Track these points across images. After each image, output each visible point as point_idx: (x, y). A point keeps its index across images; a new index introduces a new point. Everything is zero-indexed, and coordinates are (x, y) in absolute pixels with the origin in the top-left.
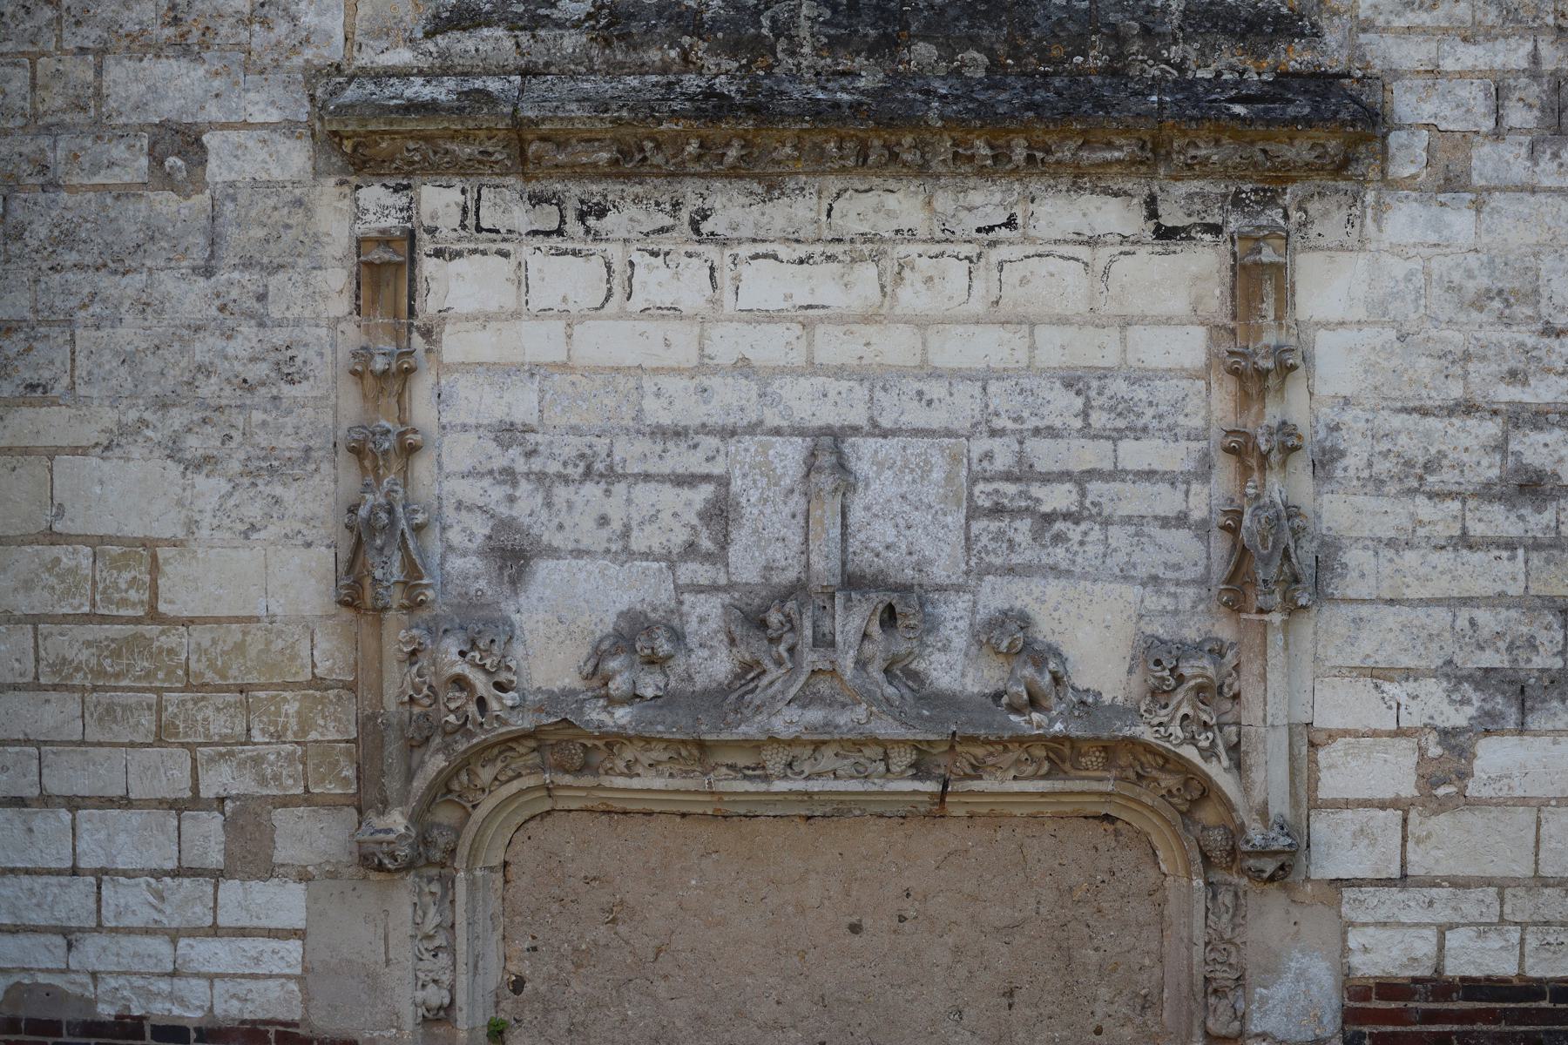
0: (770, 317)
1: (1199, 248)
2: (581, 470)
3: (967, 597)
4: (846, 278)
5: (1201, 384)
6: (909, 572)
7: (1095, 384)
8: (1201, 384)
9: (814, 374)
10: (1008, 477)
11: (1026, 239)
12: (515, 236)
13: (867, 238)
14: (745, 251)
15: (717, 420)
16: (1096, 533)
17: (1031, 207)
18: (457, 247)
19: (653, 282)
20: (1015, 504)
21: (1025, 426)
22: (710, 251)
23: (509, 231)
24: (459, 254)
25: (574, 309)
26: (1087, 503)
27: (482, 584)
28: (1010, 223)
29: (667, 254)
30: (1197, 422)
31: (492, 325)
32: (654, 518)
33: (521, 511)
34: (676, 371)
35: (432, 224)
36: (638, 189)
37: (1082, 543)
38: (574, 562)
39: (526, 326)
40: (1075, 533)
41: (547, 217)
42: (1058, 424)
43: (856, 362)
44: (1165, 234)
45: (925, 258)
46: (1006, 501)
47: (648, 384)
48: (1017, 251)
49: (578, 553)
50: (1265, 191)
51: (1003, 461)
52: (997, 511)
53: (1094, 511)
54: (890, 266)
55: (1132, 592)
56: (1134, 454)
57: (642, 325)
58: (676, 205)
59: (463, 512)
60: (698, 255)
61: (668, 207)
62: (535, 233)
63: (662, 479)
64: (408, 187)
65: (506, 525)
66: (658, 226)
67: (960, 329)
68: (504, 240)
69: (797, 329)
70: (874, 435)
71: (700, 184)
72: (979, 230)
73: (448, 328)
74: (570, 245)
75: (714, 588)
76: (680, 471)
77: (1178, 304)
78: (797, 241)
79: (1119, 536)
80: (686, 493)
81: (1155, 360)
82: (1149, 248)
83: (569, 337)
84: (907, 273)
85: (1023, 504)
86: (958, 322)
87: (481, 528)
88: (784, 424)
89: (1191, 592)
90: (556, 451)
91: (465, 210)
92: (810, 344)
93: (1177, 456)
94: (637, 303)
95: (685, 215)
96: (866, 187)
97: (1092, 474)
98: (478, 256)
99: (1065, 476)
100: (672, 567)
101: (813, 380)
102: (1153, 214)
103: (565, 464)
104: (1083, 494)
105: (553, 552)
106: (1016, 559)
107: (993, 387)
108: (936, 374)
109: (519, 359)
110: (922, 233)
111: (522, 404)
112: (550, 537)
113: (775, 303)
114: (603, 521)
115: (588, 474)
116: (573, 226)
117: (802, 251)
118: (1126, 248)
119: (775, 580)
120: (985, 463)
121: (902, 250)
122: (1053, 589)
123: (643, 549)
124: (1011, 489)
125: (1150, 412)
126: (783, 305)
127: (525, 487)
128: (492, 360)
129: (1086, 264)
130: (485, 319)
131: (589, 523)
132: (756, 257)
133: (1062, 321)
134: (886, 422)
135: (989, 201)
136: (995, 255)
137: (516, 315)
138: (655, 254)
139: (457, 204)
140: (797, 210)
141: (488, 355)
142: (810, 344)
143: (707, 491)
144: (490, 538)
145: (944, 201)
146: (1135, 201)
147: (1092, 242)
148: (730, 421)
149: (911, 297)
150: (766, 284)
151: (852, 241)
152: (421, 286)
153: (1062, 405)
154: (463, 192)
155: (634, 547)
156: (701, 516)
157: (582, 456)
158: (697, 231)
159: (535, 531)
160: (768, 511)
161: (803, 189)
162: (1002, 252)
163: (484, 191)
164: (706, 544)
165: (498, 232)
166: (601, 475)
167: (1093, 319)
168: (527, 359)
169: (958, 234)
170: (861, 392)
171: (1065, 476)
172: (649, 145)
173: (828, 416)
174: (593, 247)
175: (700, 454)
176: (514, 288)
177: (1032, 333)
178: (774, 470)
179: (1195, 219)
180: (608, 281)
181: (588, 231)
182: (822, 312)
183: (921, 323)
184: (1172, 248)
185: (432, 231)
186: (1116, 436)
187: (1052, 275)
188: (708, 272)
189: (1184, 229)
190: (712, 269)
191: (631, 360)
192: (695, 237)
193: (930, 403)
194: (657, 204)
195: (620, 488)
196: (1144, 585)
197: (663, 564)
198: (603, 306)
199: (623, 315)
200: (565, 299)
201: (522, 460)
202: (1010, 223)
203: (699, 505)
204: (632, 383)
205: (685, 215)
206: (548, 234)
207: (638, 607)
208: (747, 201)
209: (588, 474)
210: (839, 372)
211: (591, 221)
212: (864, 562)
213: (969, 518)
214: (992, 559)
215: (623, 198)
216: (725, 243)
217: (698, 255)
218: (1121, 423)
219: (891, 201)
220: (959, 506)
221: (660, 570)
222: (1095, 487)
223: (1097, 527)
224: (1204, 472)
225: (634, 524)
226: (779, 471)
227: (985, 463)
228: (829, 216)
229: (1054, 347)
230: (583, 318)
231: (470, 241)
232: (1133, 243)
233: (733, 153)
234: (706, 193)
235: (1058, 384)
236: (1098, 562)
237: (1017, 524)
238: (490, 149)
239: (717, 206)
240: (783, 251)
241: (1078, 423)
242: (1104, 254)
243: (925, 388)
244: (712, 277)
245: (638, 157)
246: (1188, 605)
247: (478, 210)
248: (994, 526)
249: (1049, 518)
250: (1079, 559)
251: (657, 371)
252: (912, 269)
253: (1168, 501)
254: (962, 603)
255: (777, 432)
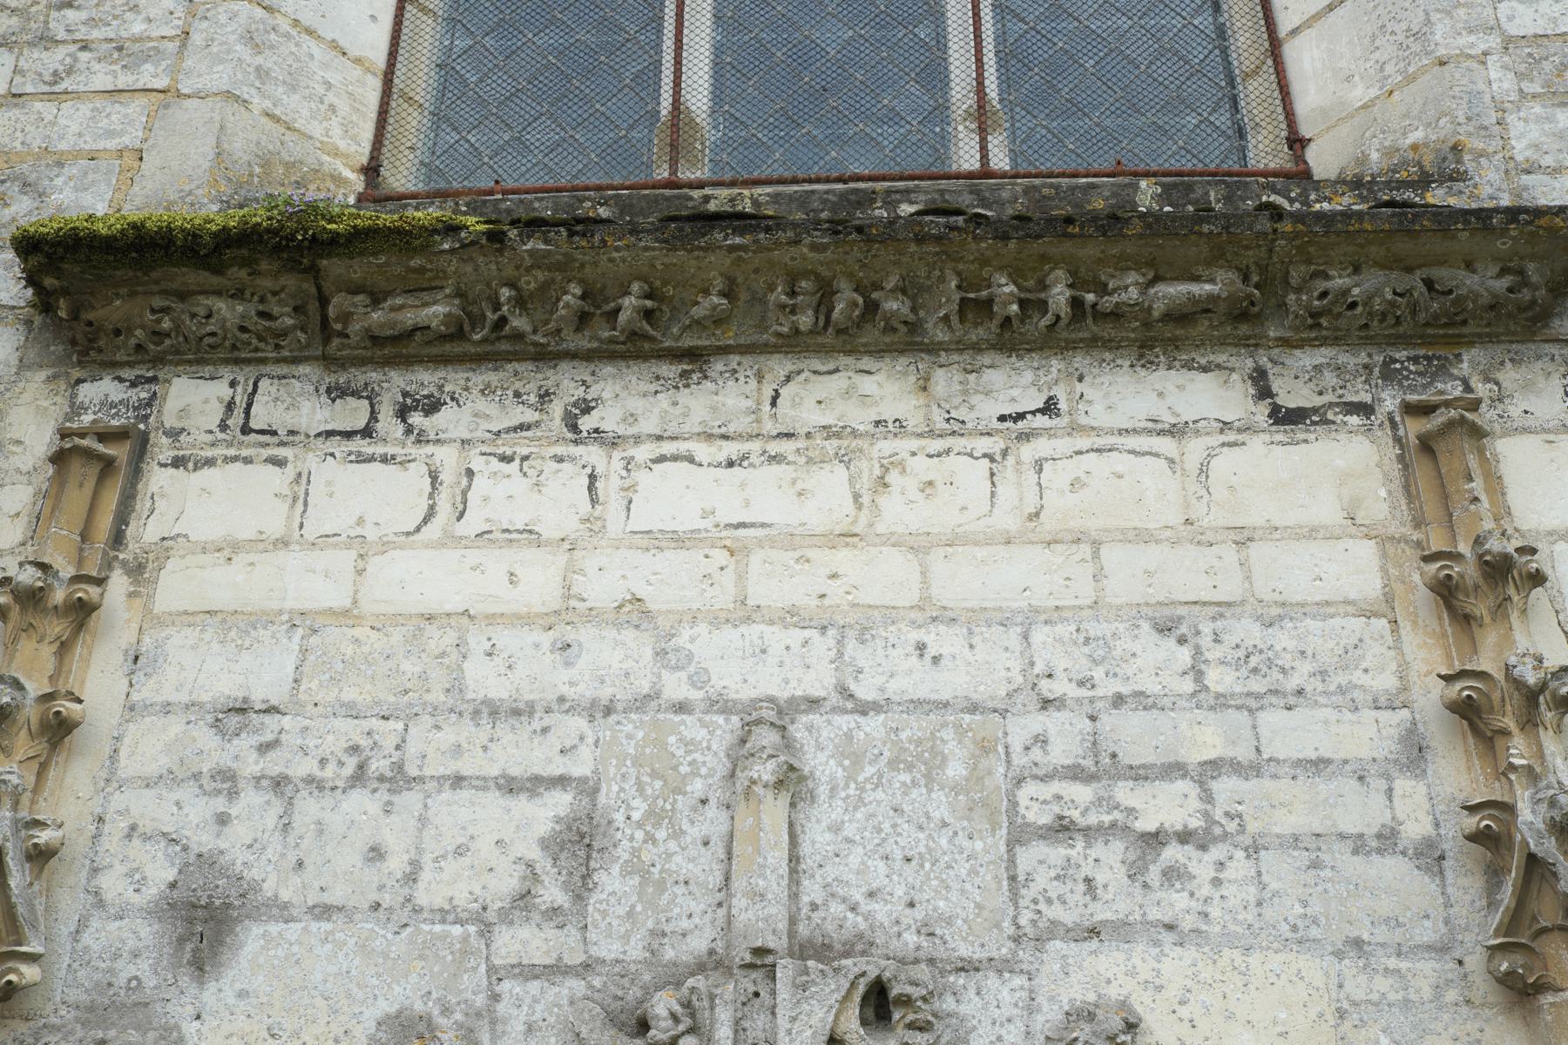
0: (679, 540)
1: (1342, 436)
2: (349, 770)
3: (1019, 981)
4: (799, 486)
5: (1381, 624)
6: (911, 938)
7: (1207, 629)
8: (1381, 624)
9: (748, 620)
10: (1075, 773)
11: (1075, 429)
12: (297, 439)
13: (829, 432)
14: (643, 452)
15: (585, 690)
16: (1239, 867)
17: (1079, 387)
18: (209, 453)
19: (501, 494)
20: (1092, 819)
21: (1099, 692)
22: (592, 454)
23: (292, 433)
24: (210, 462)
25: (371, 533)
26: (1218, 815)
27: (143, 968)
28: (1049, 408)
29: (525, 458)
30: (1386, 681)
31: (241, 559)
32: (460, 851)
33: (233, 845)
34: (524, 620)
35: (178, 425)
36: (493, 377)
37: (1216, 882)
38: (314, 926)
39: (292, 559)
40: (1201, 865)
41: (353, 413)
42: (1151, 686)
43: (815, 602)
44: (1286, 418)
45: (921, 458)
46: (1075, 814)
47: (477, 642)
48: (1063, 445)
49: (325, 911)
50: (1426, 357)
51: (1062, 752)
52: (1062, 829)
53: (1232, 827)
54: (867, 470)
55: (1314, 968)
56: (1288, 735)
57: (474, 556)
58: (545, 396)
59: (136, 842)
60: (573, 459)
61: (533, 399)
62: (329, 434)
63: (483, 784)
64: (154, 380)
65: (207, 861)
66: (515, 422)
67: (980, 553)
68: (282, 444)
69: (721, 557)
70: (845, 711)
71: (583, 371)
72: (1002, 418)
73: (170, 565)
74: (380, 450)
75: (555, 971)
76: (515, 771)
77: (1328, 512)
78: (725, 437)
79: (1281, 869)
80: (521, 805)
81: (1299, 587)
82: (1266, 437)
83: (360, 572)
84: (893, 477)
85: (1107, 819)
86: (976, 543)
87: (161, 872)
88: (695, 695)
89: (1427, 970)
90: (311, 743)
91: (230, 406)
92: (741, 577)
93: (1369, 736)
94: (474, 522)
95: (557, 409)
96: (831, 367)
97: (1214, 767)
98: (238, 464)
99: (1174, 770)
100: (486, 930)
101: (743, 629)
102: (1264, 392)
103: (323, 762)
104: (1208, 797)
105: (282, 911)
106: (1101, 913)
107: (1039, 635)
108: (943, 617)
109: (275, 605)
110: (915, 421)
111: (264, 672)
112: (275, 884)
113: (689, 521)
114: (376, 853)
115: (359, 777)
116: (388, 424)
117: (732, 449)
118: (1231, 437)
119: (669, 954)
120: (1036, 753)
121: (886, 447)
122: (1176, 964)
123: (439, 902)
124: (1082, 793)
125: (1306, 667)
126: (703, 524)
127: (251, 798)
128: (231, 608)
129: (1171, 461)
130: (230, 549)
131: (350, 858)
132: (662, 459)
133: (1143, 537)
134: (865, 691)
135: (1012, 385)
136: (1028, 452)
137: (283, 543)
138: (505, 459)
139: (220, 400)
140: (727, 396)
141: (221, 599)
142: (741, 577)
143: (560, 802)
144: (173, 885)
145: (945, 381)
146: (1235, 376)
147: (1176, 431)
148: (605, 693)
149: (900, 510)
150: (674, 495)
151: (808, 435)
152: (142, 505)
153: (1155, 663)
154: (233, 384)
155: (422, 898)
156: (545, 844)
157: (354, 749)
158: (574, 428)
159: (254, 874)
160: (661, 834)
161: (735, 371)
162: (1041, 447)
163: (264, 384)
164: (552, 893)
165: (274, 433)
166: (382, 779)
167: (1192, 533)
168: (288, 605)
169: (970, 425)
170: (822, 646)
171: (1174, 770)
172: (505, 293)
173: (770, 682)
174: (414, 451)
175: (554, 741)
176: (286, 506)
177: (1096, 555)
178: (675, 768)
179: (1329, 398)
180: (431, 496)
181: (409, 430)
182: (760, 532)
183: (918, 546)
184: (1301, 436)
185: (174, 434)
186: (1252, 704)
187: (1120, 477)
188: (587, 481)
189: (1315, 410)
190: (593, 478)
191: (454, 604)
192: (570, 436)
193: (936, 660)
194: (517, 395)
195: (411, 800)
196: (1339, 955)
197: (472, 929)
198: (418, 529)
199: (450, 540)
200: (360, 521)
201: (254, 755)
202: (1049, 408)
203: (544, 827)
204: (450, 638)
205: (557, 409)
206: (348, 435)
207: (419, 1006)
208: (653, 387)
209: (359, 777)
210: (791, 617)
211: (416, 419)
212: (835, 920)
213: (1012, 844)
214: (1055, 912)
215: (467, 389)
216: (614, 442)
217: (573, 459)
218: (1257, 685)
219: (868, 384)
220: (995, 827)
221: (465, 939)
222: (1226, 788)
223: (1240, 854)
224: (1414, 753)
225: (427, 860)
226: (684, 769)
227: (1036, 753)
228: (774, 403)
229: (1130, 574)
230: (385, 546)
231: (230, 444)
232: (1239, 431)
233: (630, 304)
234: (589, 379)
235: (1146, 626)
236: (1250, 917)
237: (1098, 850)
238: (276, 310)
239: (605, 395)
240: (702, 450)
241: (1188, 686)
242: (1195, 448)
243: (929, 639)
244: (591, 488)
245: (491, 317)
246: (1427, 993)
247: (249, 405)
248: (1056, 853)
249: (1155, 840)
250: (1215, 912)
251: (492, 619)
252: (904, 470)
253: (1360, 811)
254: (1005, 991)
255: (681, 707)
